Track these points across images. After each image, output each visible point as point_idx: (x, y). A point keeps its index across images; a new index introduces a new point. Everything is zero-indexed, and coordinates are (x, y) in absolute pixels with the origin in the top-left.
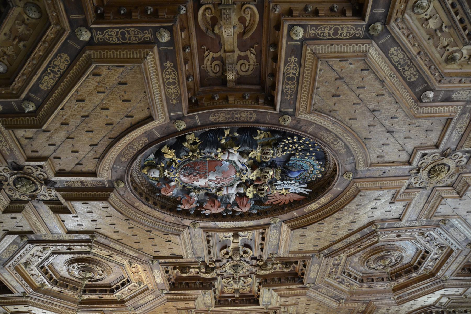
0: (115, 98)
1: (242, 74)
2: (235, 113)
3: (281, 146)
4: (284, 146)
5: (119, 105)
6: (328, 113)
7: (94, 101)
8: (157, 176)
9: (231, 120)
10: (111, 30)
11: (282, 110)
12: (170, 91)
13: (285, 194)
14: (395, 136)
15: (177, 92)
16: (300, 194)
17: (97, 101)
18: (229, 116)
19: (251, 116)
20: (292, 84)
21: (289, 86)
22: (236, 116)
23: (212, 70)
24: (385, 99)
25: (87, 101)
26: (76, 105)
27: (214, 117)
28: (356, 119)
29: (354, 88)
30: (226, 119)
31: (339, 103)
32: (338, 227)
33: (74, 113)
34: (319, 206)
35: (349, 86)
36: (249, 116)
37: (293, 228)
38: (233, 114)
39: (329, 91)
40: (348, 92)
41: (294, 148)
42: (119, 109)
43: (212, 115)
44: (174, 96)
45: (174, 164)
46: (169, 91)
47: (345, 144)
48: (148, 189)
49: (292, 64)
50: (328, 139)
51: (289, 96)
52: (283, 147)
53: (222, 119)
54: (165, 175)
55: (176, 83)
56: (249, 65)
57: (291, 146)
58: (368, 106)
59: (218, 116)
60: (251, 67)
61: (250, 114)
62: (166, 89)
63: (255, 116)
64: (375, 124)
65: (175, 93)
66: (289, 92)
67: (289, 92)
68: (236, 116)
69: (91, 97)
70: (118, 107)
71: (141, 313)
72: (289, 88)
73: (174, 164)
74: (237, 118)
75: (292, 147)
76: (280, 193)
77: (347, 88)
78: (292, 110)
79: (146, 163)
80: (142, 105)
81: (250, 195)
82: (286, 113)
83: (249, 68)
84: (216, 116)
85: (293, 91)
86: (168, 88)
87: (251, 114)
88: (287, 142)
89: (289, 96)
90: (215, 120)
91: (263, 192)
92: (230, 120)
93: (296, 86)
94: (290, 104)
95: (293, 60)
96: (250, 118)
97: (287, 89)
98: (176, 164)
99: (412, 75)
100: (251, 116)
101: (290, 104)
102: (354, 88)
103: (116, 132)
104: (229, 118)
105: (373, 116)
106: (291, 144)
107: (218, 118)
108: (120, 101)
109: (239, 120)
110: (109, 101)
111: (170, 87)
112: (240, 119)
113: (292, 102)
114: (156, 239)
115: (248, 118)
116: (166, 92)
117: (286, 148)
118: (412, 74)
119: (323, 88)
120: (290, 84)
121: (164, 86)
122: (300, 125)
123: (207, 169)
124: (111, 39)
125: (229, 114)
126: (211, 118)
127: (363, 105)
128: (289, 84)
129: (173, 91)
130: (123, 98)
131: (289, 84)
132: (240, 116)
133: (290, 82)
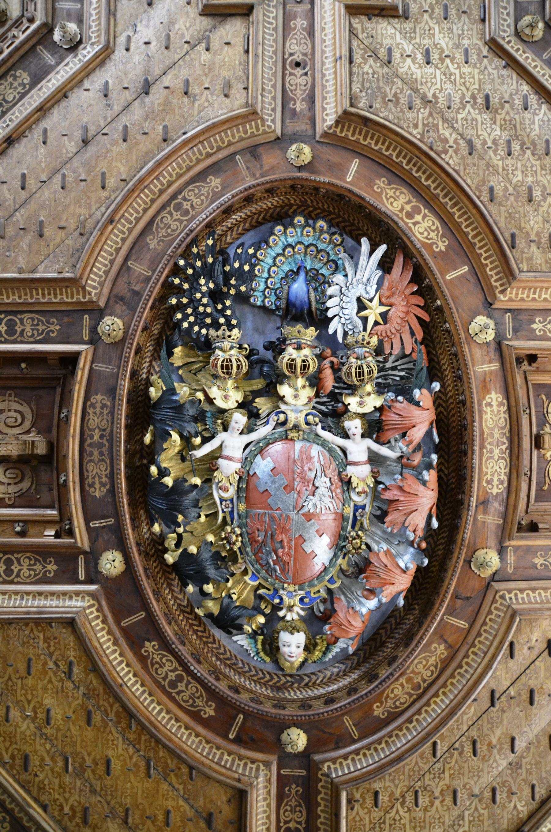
0: (22, 688)
1: (27, 424)
2: (89, 441)
3: (204, 331)
4: (203, 325)
5: (40, 686)
6: (84, 239)
7: (28, 733)
8: (300, 638)
9: (105, 450)
11: (86, 338)
12: (25, 572)
13: (384, 309)
14: (157, 72)
15: (30, 559)
16: (385, 265)
17: (28, 727)
18: (96, 453)
19: (98, 405)
20: (22, 323)
21: (28, 328)
22: (96, 438)
23: (15, 484)
24: (459, 67)
25: (27, 749)
26: (36, 775)
27: (97, 486)
28: (104, 174)
29: (24, 195)
30: (103, 460)
31: (60, 219)
32: (509, 142)
33: (57, 787)
34: (424, 211)
35: (17, 206)
36: (98, 410)
37: (509, 274)
38: (90, 445)
39: (30, 245)
40: (33, 205)
41: (205, 301)
42: (50, 686)
43: (92, 490)
44: (38, 567)
45: (261, 591)
46: (26, 575)
47: (193, 180)
48: (353, 669)
51: (52, 328)
52: (208, 326)
53: (103, 469)
54: (296, 617)
55: (9, 559)
56: (9, 410)
57: (201, 309)
58: (70, 155)
59: (94, 478)
60: (15, 406)
61: (95, 408)
62: (19, 579)
63: (99, 397)
64: (121, 128)
65: (32, 562)
66: (41, 327)
67: (41, 327)
68: (96, 438)
69: (18, 738)
70: (45, 689)
72: (33, 330)
73: (261, 591)
74: (102, 437)
75: (205, 306)
76: (376, 323)
77: (23, 211)
78: (86, 316)
79: (267, 659)
80: (42, 636)
81: (373, 402)
82: (94, 330)
83: (16, 411)
84: (94, 483)
85: (39, 320)
86: (18, 575)
87: (93, 406)
88: (192, 319)
89: (52, 328)
90: (103, 485)
91: (366, 369)
92: (106, 453)
93: (27, 315)
94: (70, 324)
96: (102, 408)
97: (35, 333)
98: (260, 586)
99: (16, 84)
100: (98, 405)
101: (70, 324)
102: (24, 195)
103: (111, 706)
104: (101, 454)
105: (100, 136)
106: (195, 309)
107: (100, 477)
108: (30, 681)
109: (108, 431)
110: (29, 702)
111: (16, 571)
112: (104, 430)
113: (66, 319)
114: (532, 683)
115: (101, 413)
116: (28, 580)
117: (208, 321)
118: (11, 84)
119: (20, 259)
120: (22, 327)
121: (11, 582)
122: (128, 295)
123: (262, 511)
124: (398, 703)
125: (91, 454)
126: (97, 494)
127: (68, 166)
128: (23, 330)
129: (25, 568)
130: (24, 674)
131: (23, 330)
132: (97, 431)
133: (18, 329)
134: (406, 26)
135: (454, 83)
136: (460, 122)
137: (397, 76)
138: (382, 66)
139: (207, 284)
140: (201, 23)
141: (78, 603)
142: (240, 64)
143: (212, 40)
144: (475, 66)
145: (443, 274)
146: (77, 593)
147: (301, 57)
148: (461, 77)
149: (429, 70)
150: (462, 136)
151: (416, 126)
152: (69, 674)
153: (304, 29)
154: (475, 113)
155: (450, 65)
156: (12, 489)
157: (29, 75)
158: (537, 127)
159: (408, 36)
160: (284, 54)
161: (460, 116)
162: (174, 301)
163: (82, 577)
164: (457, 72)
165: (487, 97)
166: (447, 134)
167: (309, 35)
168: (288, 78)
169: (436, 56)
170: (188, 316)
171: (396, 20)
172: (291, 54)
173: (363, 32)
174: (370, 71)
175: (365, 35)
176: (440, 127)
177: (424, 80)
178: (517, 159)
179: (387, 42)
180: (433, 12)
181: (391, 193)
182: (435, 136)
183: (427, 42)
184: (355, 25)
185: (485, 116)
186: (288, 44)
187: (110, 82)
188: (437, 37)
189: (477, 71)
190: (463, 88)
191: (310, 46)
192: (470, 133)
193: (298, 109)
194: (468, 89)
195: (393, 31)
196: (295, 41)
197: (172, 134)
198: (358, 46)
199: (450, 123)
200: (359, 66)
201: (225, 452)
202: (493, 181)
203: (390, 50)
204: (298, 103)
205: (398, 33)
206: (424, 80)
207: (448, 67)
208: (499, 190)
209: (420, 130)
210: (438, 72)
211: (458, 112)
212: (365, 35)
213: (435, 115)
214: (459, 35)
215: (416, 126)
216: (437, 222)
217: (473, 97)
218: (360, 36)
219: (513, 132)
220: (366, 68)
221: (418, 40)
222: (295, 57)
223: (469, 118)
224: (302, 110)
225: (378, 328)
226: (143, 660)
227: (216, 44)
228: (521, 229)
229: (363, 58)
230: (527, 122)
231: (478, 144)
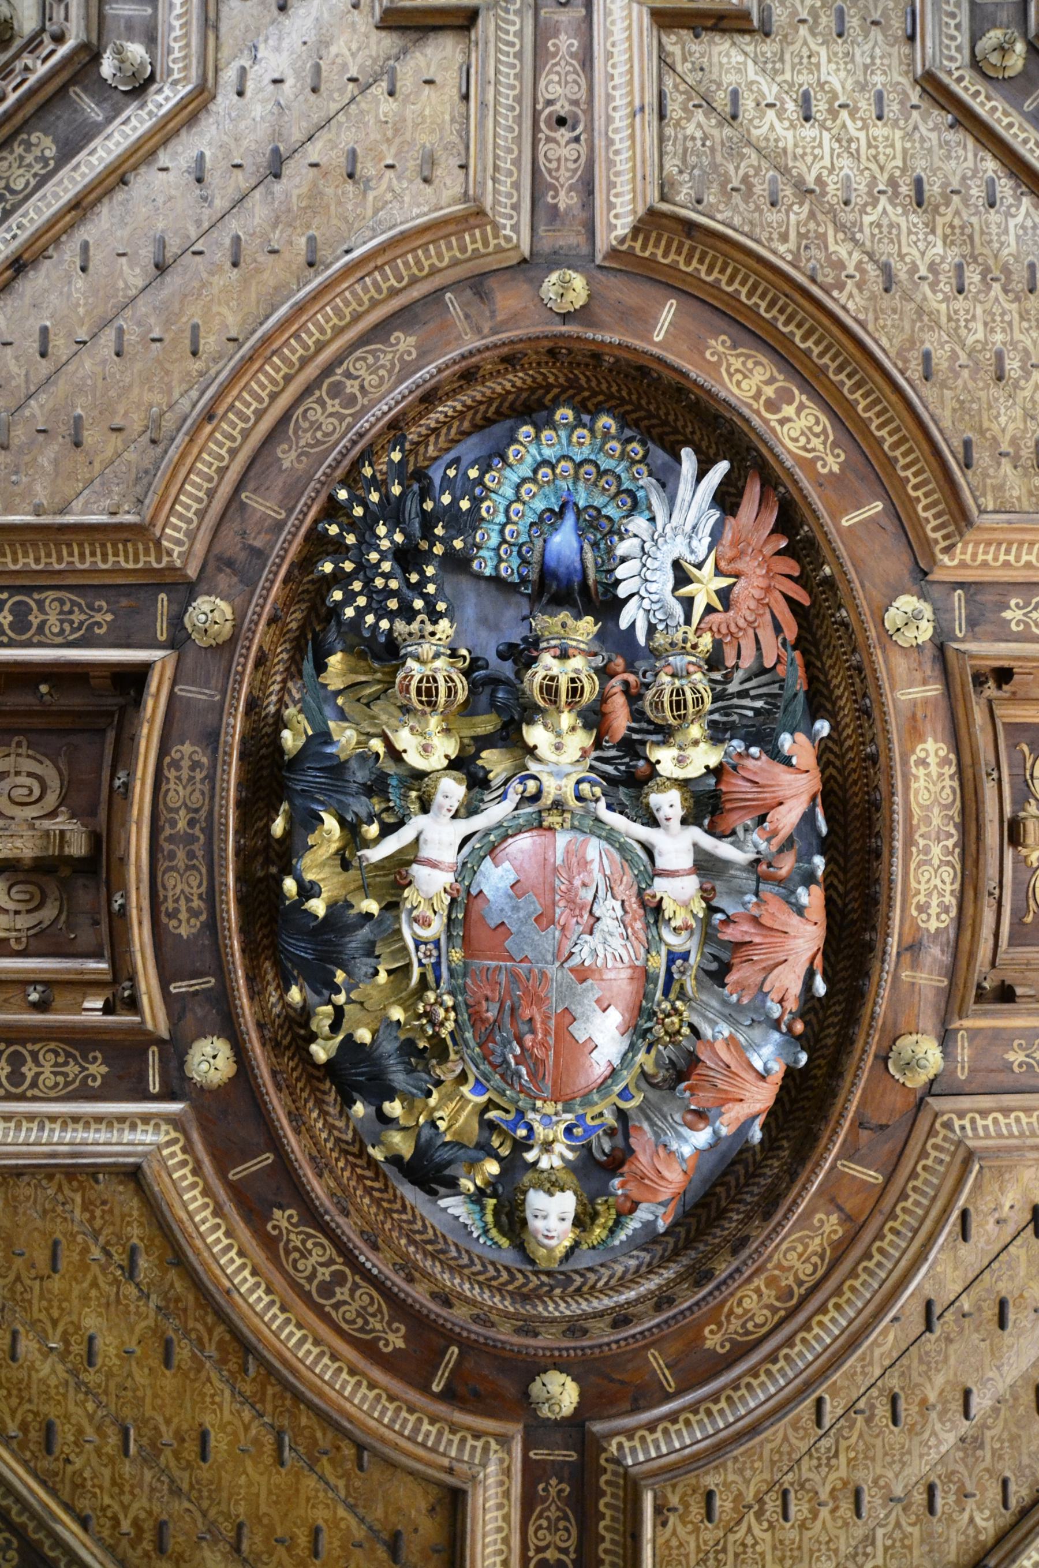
0: (42, 1297)
1: (52, 799)
2: (168, 831)
3: (384, 624)
4: (382, 613)
5: (75, 1293)
6: (159, 450)
7: (53, 1381)
8: (566, 1203)
9: (198, 848)
10: (820, 1273)
11: (162, 637)
12: (47, 1077)
13: (724, 582)
14: (297, 135)
15: (57, 1054)
16: (726, 500)
17: (54, 1371)
18: (181, 854)
19: (186, 764)
20: (42, 609)
21: (53, 619)
22: (182, 825)
23: (28, 912)
25: (51, 1411)
26: (68, 1461)
27: (183, 915)
28: (195, 328)
29: (45, 367)
30: (194, 867)
31: (114, 413)
32: (959, 268)
33: (107, 1483)
34: (800, 397)
35: (33, 389)
36: (185, 773)
37: (959, 517)
38: (170, 839)
39: (56, 462)
40: (62, 386)
41: (386, 566)
42: (94, 1293)
43: (174, 923)
44: (72, 1069)
45: (492, 1115)
46: (50, 1083)
47: (364, 340)
48: (665, 1261)
49: (83, 617)
50: (805, 421)
51: (98, 618)
52: (391, 615)
53: (195, 884)
54: (557, 1163)
55: (16, 1053)
56: (17, 773)
57: (379, 582)
58: (133, 292)
59: (177, 901)
60: (28, 765)
61: (178, 768)
62: (36, 1092)
63: (187, 748)
64: (227, 242)
65: (61, 1060)
66: (77, 617)
67: (77, 617)
68: (182, 825)
69: (34, 1390)
70: (85, 1298)
71: (10, 1491)
72: (62, 622)
73: (492, 1115)
74: (191, 823)
75: (387, 576)
76: (710, 609)
77: (43, 397)
78: (163, 596)
79: (504, 1242)
80: (78, 1200)
81: (704, 757)
82: (177, 622)
83: (30, 774)
84: (177, 911)
85: (73, 603)
86: (34, 1084)
87: (176, 765)
88: (362, 601)
89: (98, 618)
90: (194, 913)
91: (689, 696)
92: (200, 853)
93: (51, 594)
94: (133, 611)
95: (1019, 614)
96: (192, 768)
97: (67, 627)
98: (491, 1104)
99: (29, 159)
100: (186, 764)
101: (133, 611)
102: (45, 367)
103: (210, 1331)
104: (191, 855)
105: (188, 257)
106: (368, 582)
107: (188, 900)
108: (56, 1284)
109: (203, 813)
110: (55, 1323)
111: (30, 1075)
112: (196, 811)
113: (124, 602)
114: (1004, 1288)
115: (191, 779)
116: (52, 1094)
117: (393, 604)
118: (21, 158)
119: (38, 488)
120: (42, 617)
121: (22, 1098)
122: (242, 556)
123: (493, 964)
125: (172, 856)
126: (184, 931)
127: (128, 312)
128: (44, 623)
129: (47, 1070)
130: (46, 1271)
131: (44, 623)
132: (182, 812)
133: (35, 619)
134: (765, 48)
135: (856, 156)
136: (867, 231)
137: (749, 143)
138: (720, 125)
139: (389, 535)
140: (379, 43)
141: (146, 1137)
142: (453, 120)
143: (399, 75)
144: (895, 124)
145: (835, 517)
146: (146, 1118)
147: (567, 107)
148: (869, 146)
149: (809, 131)
150: (871, 255)
151: (784, 238)
152: (131, 1270)
153: (573, 55)
154: (895, 213)
155: (849, 123)
156: (23, 922)
157: (55, 141)
158: (1012, 239)
159: (770, 68)
160: (535, 101)
161: (867, 219)
162: (328, 567)
163: (154, 1087)
164: (862, 135)
165: (918, 183)
166: (843, 253)
167: (583, 66)
168: (542, 148)
169: (823, 106)
170: (354, 595)
171: (747, 38)
172: (549, 103)
173: (685, 60)
174: (699, 134)
175: (689, 65)
176: (831, 240)
177: (799, 151)
178: (976, 299)
179: (730, 79)
180: (816, 22)
181: (737, 364)
182: (821, 255)
183: (805, 79)
184: (669, 48)
185: (914, 218)
186: (542, 83)
187: (208, 154)
188: (823, 69)
189: (899, 134)
190: (874, 166)
191: (584, 86)
192: (886, 250)
193: (562, 206)
194: (882, 168)
195: (741, 58)
196: (556, 78)
197: (324, 253)
198: (676, 86)
199: (848, 232)
200: (678, 124)
201: (425, 853)
202: (930, 341)
203: (735, 95)
204: (562, 194)
205: (750, 63)
206: (799, 151)
207: (844, 126)
208: (940, 358)
209: (792, 244)
210: (826, 135)
211: (863, 211)
212: (689, 65)
213: (820, 217)
214: (866, 67)
215: (784, 238)
216: (823, 418)
217: (893, 182)
218: (679, 68)
219: (967, 250)
220: (691, 129)
221: (787, 76)
222: (557, 107)
223: (885, 222)
224: (569, 207)
225: (713, 618)
226: (270, 1243)
227: (406, 82)
228: (982, 432)
229: (685, 109)
230: (994, 229)
231: (901, 271)
